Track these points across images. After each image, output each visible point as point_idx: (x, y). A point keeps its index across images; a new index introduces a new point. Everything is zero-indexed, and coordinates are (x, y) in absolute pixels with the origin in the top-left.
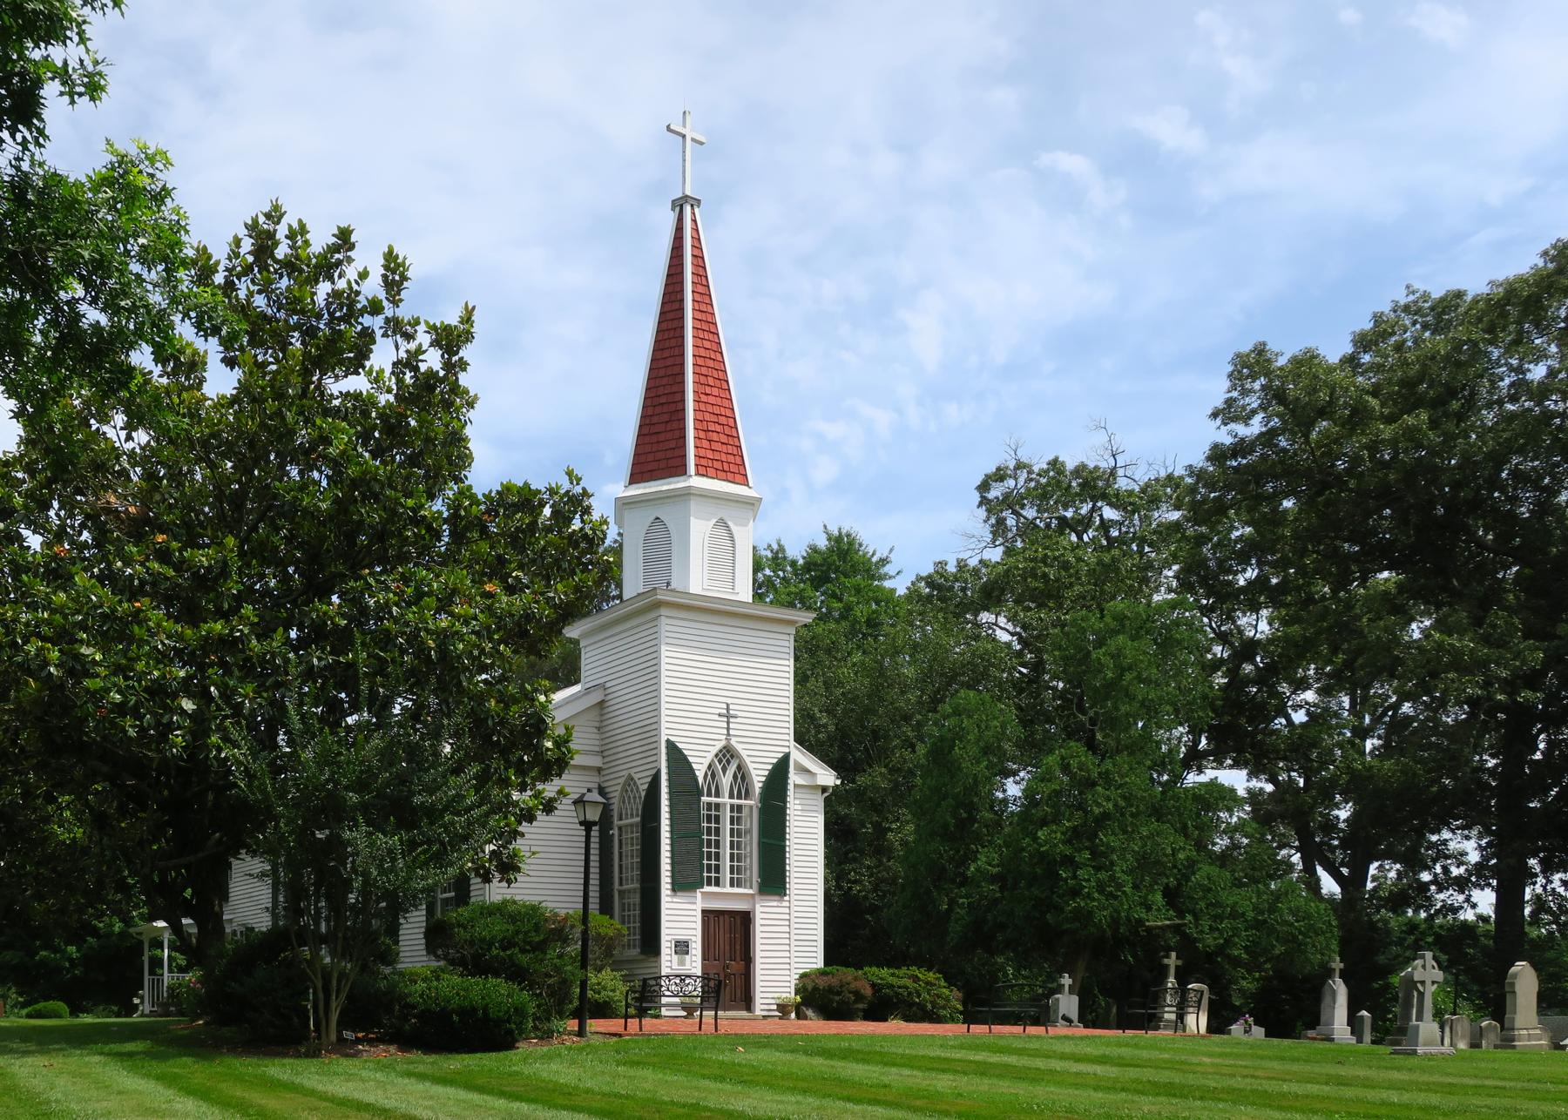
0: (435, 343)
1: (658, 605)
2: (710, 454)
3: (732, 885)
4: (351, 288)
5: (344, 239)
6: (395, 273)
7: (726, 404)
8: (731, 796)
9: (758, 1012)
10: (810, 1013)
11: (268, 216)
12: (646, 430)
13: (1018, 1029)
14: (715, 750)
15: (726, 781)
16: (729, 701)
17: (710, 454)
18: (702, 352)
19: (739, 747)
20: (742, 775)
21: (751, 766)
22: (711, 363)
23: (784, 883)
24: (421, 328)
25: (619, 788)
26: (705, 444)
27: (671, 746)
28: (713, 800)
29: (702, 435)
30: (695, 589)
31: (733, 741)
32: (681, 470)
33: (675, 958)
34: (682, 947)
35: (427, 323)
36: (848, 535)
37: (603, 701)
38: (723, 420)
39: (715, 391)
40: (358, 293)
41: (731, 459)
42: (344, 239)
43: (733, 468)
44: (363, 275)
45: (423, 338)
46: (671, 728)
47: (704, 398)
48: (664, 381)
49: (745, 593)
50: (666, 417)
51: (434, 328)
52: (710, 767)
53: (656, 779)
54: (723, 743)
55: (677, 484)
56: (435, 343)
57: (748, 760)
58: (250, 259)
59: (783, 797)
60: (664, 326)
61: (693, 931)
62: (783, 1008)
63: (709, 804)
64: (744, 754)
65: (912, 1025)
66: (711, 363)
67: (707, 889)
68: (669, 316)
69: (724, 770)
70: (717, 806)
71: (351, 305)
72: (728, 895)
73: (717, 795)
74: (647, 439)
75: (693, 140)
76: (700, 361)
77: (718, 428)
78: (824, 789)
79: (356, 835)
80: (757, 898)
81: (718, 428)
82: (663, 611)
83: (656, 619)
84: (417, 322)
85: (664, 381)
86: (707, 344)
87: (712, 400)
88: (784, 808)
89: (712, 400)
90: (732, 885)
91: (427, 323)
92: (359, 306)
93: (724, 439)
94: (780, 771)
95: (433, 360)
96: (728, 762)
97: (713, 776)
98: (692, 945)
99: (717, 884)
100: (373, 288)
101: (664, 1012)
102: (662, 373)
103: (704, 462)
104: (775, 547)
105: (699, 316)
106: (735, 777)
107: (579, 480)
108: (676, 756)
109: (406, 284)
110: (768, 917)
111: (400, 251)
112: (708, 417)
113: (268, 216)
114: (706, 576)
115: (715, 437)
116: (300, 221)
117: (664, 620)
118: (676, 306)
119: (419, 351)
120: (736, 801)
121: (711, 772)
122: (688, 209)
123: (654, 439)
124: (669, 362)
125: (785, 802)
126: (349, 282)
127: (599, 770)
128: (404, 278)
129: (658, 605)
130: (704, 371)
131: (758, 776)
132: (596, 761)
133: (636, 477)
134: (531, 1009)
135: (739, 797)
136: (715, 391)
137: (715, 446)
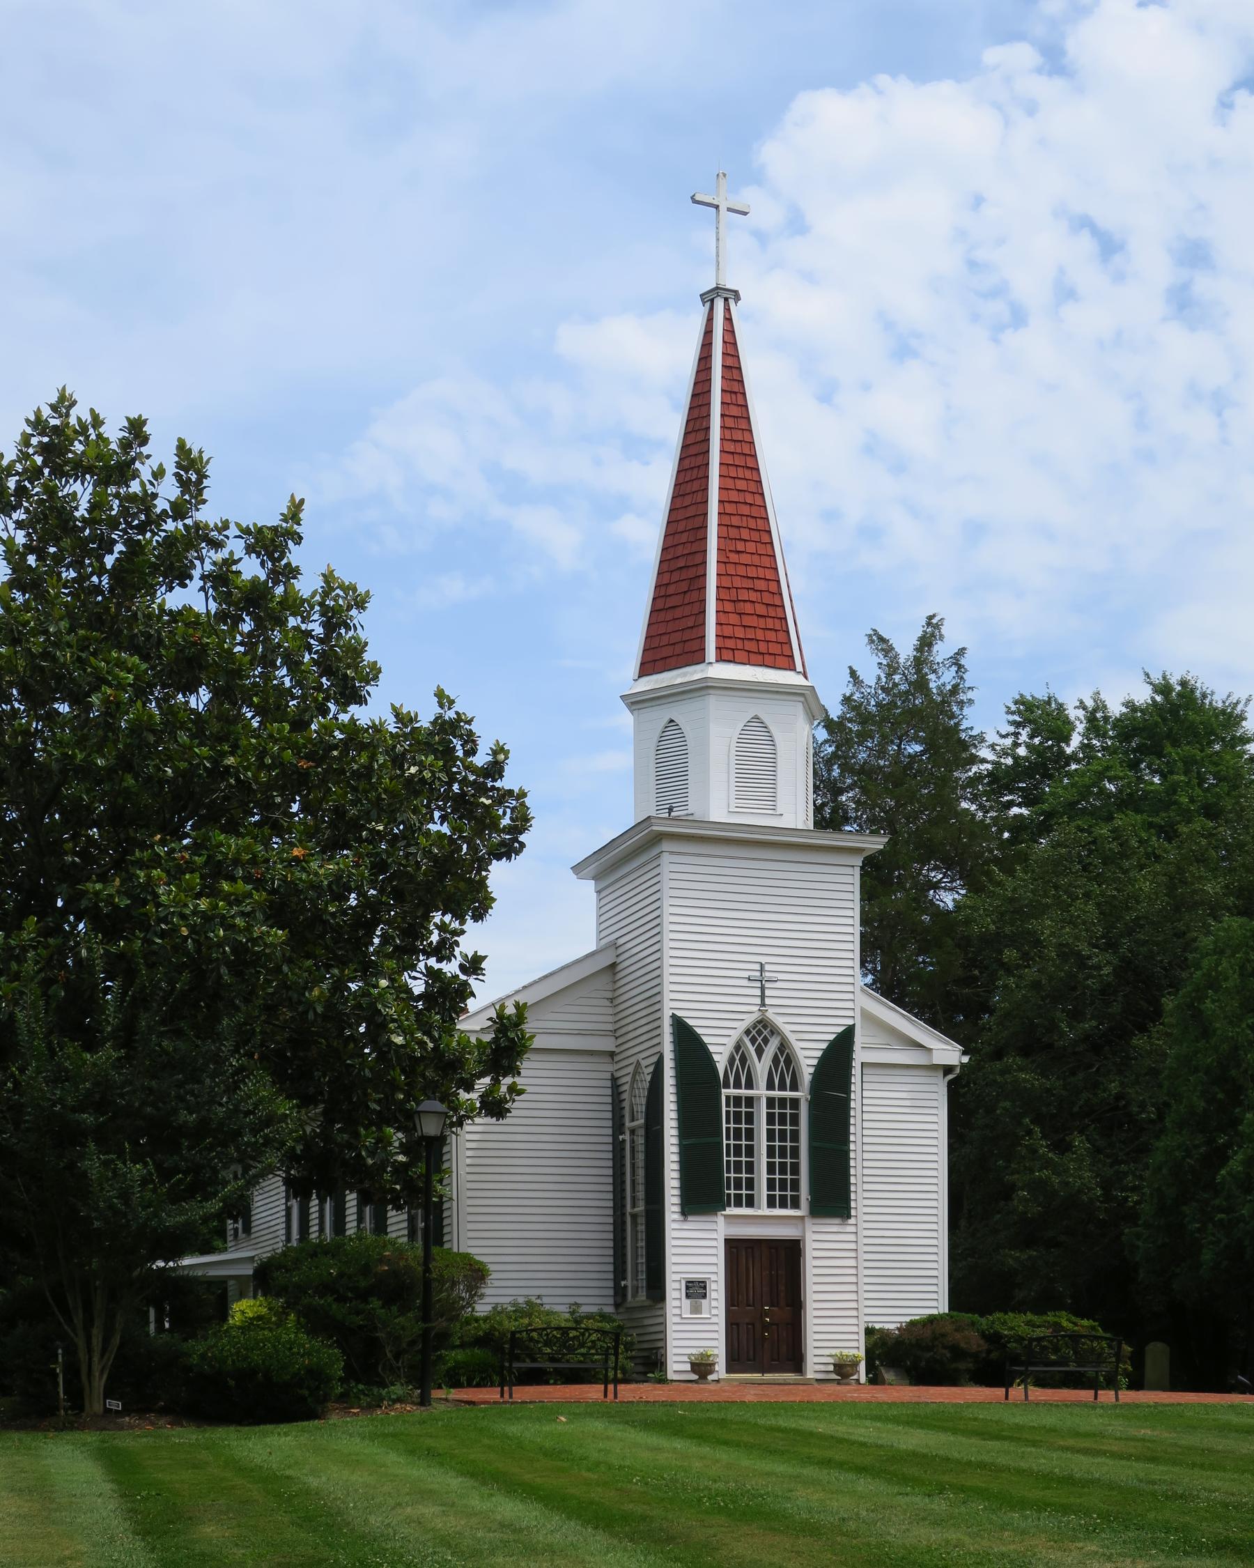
0: (250, 549)
1: (658, 838)
2: (740, 633)
3: (771, 1204)
4: (145, 491)
5: (137, 431)
6: (191, 467)
7: (766, 561)
8: (770, 1086)
9: (810, 1375)
10: (889, 1376)
11: (54, 408)
12: (660, 605)
13: (1086, 1395)
14: (742, 1026)
15: (761, 1068)
16: (763, 959)
17: (740, 633)
18: (734, 496)
19: (779, 1021)
20: (785, 1058)
21: (797, 1046)
22: (745, 510)
23: (848, 1200)
24: (233, 531)
25: (628, 1079)
26: (734, 619)
27: (681, 1028)
28: (743, 1092)
29: (729, 607)
30: (718, 813)
31: (771, 1014)
32: (697, 657)
33: (687, 1303)
34: (696, 1290)
35: (238, 525)
36: (1184, 683)
37: (614, 965)
38: (761, 585)
39: (751, 547)
40: (155, 496)
41: (771, 636)
42: (137, 431)
43: (774, 648)
44: (158, 474)
45: (236, 546)
46: (674, 1003)
47: (734, 557)
48: (684, 538)
49: (794, 808)
50: (684, 586)
51: (246, 531)
52: (738, 1047)
53: (659, 1065)
54: (755, 1017)
55: (693, 673)
56: (250, 549)
57: (792, 1038)
58: (39, 460)
59: (844, 1084)
60: (687, 463)
61: (714, 1270)
62: (843, 1369)
63: (737, 1100)
64: (786, 1029)
65: (1049, 1391)
66: (745, 510)
67: (732, 1211)
68: (693, 450)
69: (760, 1052)
70: (750, 1101)
71: (148, 509)
72: (763, 1221)
73: (749, 1085)
74: (662, 616)
75: (729, 210)
76: (730, 508)
77: (753, 596)
78: (947, 1069)
79: (93, 1163)
80: (808, 1221)
81: (753, 596)
82: (666, 846)
83: (658, 856)
84: (226, 525)
85: (684, 538)
86: (741, 485)
87: (745, 559)
88: (847, 1100)
89: (745, 559)
90: (771, 1204)
91: (238, 525)
92: (158, 510)
93: (761, 610)
94: (840, 1050)
95: (251, 569)
96: (766, 1041)
97: (743, 1060)
98: (712, 1286)
99: (750, 1203)
100: (168, 491)
101: (671, 1376)
102: (681, 527)
103: (730, 643)
104: (1090, 704)
105: (731, 447)
106: (776, 1060)
107: (451, 702)
108: (686, 1037)
109: (206, 482)
110: (825, 1250)
111: (194, 445)
112: (738, 582)
113: (54, 408)
114: (733, 794)
115: (748, 608)
116: (92, 410)
117: (666, 858)
118: (700, 436)
119: (230, 562)
120: (777, 1093)
121: (739, 1056)
122: (719, 305)
123: (669, 616)
124: (691, 511)
125: (847, 1090)
126: (142, 484)
127: (612, 1054)
128: (202, 476)
129: (658, 838)
130: (735, 521)
131: (807, 1059)
132: (608, 1044)
133: (648, 666)
134: (338, 1370)
135: (782, 1087)
136: (751, 547)
137: (747, 621)
